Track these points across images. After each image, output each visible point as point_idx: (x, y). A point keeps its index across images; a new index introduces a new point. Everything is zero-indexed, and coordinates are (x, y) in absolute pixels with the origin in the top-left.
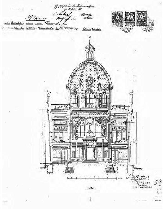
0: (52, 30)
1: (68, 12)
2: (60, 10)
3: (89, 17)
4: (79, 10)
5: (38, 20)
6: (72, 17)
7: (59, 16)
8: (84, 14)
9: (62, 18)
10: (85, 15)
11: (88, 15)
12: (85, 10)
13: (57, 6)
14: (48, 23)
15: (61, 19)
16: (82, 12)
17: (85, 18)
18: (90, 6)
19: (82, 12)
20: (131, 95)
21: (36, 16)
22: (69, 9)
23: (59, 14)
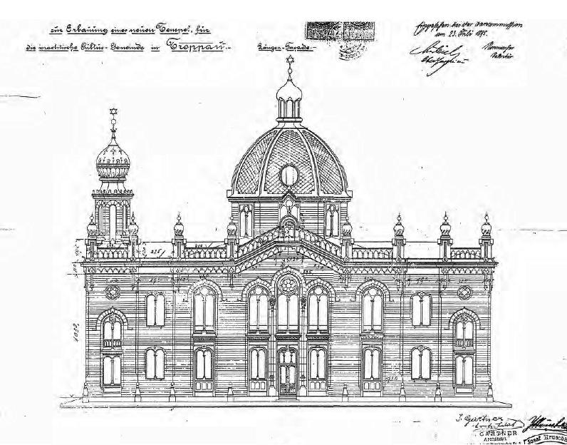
0: (305, 53)
1: (450, 43)
2: (428, 38)
3: (505, 55)
4: (478, 34)
5: (199, 45)
6: (460, 58)
7: (426, 55)
8: (491, 46)
9: (435, 59)
10: (495, 47)
11: (501, 48)
12: (499, 36)
13: (423, 26)
14: (167, 31)
15: (434, 61)
16: (485, 40)
17: (495, 56)
18: (512, 23)
19: (485, 40)
20: (486, 239)
21: (97, 185)
22: (452, 33)
23: (426, 51)
